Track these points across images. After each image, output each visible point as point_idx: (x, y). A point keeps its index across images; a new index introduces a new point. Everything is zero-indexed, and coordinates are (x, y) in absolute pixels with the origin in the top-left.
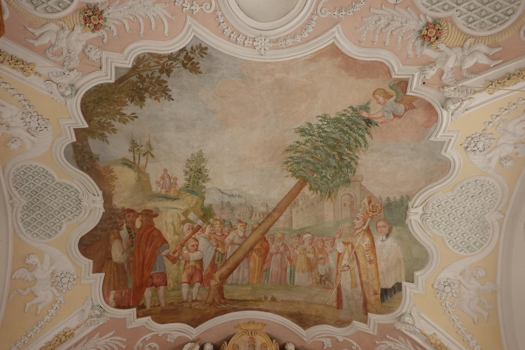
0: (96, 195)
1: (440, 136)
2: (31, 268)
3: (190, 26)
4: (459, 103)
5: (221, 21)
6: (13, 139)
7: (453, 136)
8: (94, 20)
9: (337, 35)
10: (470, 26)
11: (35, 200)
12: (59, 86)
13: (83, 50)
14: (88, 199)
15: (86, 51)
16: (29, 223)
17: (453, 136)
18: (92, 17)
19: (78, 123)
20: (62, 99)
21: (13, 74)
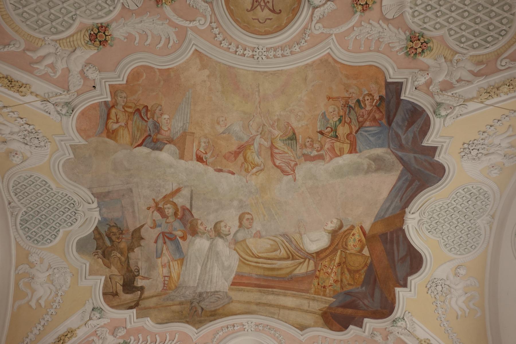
0: (91, 202)
1: (432, 141)
2: (32, 265)
3: (190, 41)
4: (450, 110)
5: (221, 39)
6: (11, 153)
7: (445, 142)
8: (101, 37)
9: (332, 46)
10: (462, 45)
11: (45, 191)
12: (56, 105)
13: (82, 70)
14: (83, 207)
15: (85, 71)
16: (38, 212)
17: (445, 142)
18: (99, 36)
19: (73, 140)
20: (59, 118)
21: (12, 96)
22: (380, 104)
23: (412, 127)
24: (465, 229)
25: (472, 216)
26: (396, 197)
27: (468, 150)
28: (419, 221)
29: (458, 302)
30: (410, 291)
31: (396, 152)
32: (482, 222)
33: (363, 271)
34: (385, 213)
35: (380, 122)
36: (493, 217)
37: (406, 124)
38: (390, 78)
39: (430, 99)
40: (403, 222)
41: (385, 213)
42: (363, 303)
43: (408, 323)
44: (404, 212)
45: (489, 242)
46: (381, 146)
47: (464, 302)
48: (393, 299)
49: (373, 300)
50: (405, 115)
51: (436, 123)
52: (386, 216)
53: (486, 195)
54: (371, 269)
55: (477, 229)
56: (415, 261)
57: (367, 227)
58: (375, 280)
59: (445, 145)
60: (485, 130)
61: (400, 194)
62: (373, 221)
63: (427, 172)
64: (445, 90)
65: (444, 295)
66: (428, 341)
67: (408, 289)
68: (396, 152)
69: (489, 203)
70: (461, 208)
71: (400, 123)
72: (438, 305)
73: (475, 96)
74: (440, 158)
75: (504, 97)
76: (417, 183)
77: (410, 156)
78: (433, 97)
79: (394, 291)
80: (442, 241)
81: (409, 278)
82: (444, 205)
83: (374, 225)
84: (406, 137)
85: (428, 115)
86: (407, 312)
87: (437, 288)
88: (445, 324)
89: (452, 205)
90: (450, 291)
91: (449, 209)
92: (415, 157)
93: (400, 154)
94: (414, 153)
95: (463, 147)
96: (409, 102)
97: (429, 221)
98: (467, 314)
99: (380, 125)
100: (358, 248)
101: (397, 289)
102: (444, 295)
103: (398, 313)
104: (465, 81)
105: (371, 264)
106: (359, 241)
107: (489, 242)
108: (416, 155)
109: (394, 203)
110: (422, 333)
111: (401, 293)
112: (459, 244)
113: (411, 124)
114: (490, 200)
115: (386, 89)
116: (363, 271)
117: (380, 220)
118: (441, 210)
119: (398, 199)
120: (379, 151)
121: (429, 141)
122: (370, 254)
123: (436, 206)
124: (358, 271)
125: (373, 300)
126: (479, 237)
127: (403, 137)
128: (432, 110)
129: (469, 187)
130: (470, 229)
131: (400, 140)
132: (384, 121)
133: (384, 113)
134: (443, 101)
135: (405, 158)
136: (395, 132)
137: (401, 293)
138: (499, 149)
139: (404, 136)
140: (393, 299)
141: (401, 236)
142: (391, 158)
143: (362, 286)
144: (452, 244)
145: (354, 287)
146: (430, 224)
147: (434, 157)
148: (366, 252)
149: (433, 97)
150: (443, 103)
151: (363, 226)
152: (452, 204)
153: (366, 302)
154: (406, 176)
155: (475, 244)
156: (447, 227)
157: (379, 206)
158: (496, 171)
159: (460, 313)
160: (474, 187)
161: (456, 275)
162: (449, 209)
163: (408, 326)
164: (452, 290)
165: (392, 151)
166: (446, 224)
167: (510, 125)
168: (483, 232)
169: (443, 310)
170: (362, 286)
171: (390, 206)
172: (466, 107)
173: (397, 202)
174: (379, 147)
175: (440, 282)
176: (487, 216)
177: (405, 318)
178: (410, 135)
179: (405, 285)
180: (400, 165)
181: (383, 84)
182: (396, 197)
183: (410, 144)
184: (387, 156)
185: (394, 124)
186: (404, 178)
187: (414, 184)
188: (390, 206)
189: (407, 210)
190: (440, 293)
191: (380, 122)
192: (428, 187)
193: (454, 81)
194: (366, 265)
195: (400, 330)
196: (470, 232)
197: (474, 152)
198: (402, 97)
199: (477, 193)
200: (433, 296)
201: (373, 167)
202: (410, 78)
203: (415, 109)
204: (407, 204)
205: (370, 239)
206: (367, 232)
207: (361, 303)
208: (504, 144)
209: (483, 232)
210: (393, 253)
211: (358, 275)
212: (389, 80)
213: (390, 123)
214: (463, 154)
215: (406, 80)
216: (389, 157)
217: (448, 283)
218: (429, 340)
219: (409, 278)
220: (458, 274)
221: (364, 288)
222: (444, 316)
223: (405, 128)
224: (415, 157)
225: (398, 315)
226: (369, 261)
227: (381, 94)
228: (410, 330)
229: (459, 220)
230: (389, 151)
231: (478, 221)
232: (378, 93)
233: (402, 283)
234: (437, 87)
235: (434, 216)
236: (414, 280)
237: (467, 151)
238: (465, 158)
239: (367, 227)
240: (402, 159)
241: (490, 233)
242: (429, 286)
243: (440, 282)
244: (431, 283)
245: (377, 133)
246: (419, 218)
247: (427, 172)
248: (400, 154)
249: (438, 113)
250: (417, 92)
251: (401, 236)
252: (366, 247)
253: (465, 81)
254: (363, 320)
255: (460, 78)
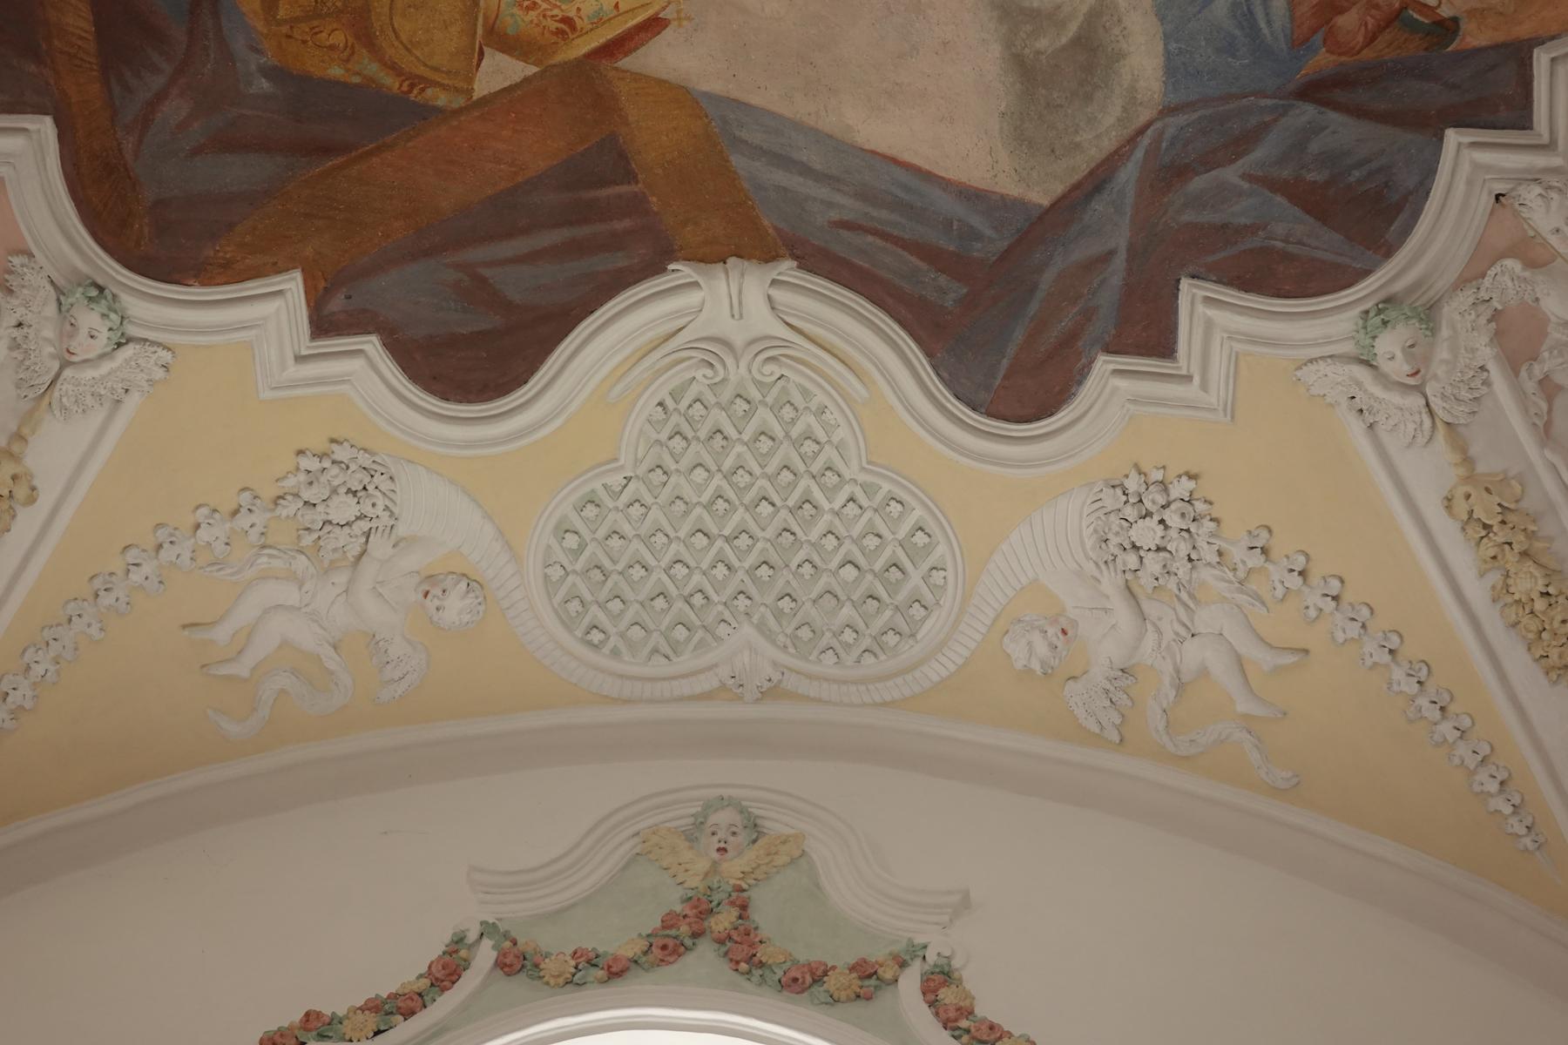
1: (1209, 325)
7: (1204, 386)
17: (1204, 386)
22: (1413, 26)
23: (1297, 211)
24: (697, 578)
25: (770, 600)
26: (864, 195)
27: (1162, 500)
28: (726, 344)
29: (284, 614)
30: (300, 359)
31: (1139, 154)
32: (746, 649)
33: (373, 69)
34: (759, 152)
35: (1319, 37)
36: (773, 692)
37: (1311, 176)
38: (1553, 60)
39: (1451, 275)
40: (711, 255)
41: (759, 152)
42: (161, 96)
43: (106, 367)
44: (767, 255)
45: (627, 701)
46: (1172, 70)
47: (285, 644)
48: (227, 265)
49: (196, 151)
50: (1359, 165)
51: (1329, 322)
52: (737, 161)
53: (891, 639)
54: (391, 114)
55: (700, 634)
56: (477, 357)
57: (663, 58)
58: (326, 150)
59: (1192, 391)
60: (1274, 554)
61: (884, 214)
62: (705, 87)
63: (1019, 335)
64: (1498, 337)
65: (308, 540)
66: (21, 492)
67: (307, 346)
68: (1139, 154)
69: (849, 659)
70: (814, 535)
71: (1314, 147)
72: (243, 521)
73: (1481, 468)
74: (1110, 385)
75: (1477, 591)
76: (950, 292)
77: (1112, 229)
78: (1460, 284)
79: (278, 270)
80: (616, 480)
81: (372, 344)
82: (829, 453)
83: (679, 95)
84: (1231, 191)
85: (1366, 273)
86: (166, 356)
87: (343, 498)
88: (147, 569)
89: (830, 492)
90: (333, 567)
91: (805, 482)
92: (1111, 253)
93: (1128, 175)
94: (1131, 248)
95: (1171, 475)
96: (1430, 171)
97: (727, 394)
98: (224, 670)
99: (1300, 43)
100: (517, 20)
101: (293, 284)
102: (308, 540)
103: (149, 304)
104: (1550, 411)
105: (427, 113)
106: (567, 20)
107: (627, 701)
108: (1122, 256)
109: (823, 192)
110: (54, 452)
111: (282, 302)
112: (607, 563)
113: (1316, 202)
114: (868, 659)
115: (1496, 47)
116: (373, 69)
117: (712, 125)
118: (797, 444)
119: (849, 206)
120: (1142, 63)
121: (1206, 313)
122: (485, 100)
123: (822, 410)
124: (366, 37)
125: (196, 151)
126: (655, 651)
127: (1230, 174)
128: (1399, 286)
129: (941, 549)
130: (698, 600)
131: (1208, 162)
132: (1321, 61)
133: (1367, 54)
134: (1445, 332)
135: (1099, 205)
136: (1264, 128)
137: (282, 302)
138: (1169, 635)
139: (1235, 180)
140: (227, 265)
141: (621, 261)
142: (1100, 129)
143: (275, 73)
144: (601, 533)
145: (260, 26)
146: (710, 398)
147: (1109, 350)
148: (499, 72)
149: (1460, 284)
150: (1434, 331)
151: (668, 34)
152: (837, 488)
153: (175, 109)
154: (988, 232)
155: (613, 641)
156: (700, 489)
157: (801, 109)
158: (1042, 649)
159: (222, 634)
160: (937, 577)
161: (430, 584)
162: (805, 482)
163: (89, 374)
164: (341, 578)
165: (1141, 131)
166: (718, 480)
167: (1306, 651)
168: (685, 662)
169: (219, 547)
170: (275, 73)
171: (806, 170)
172: (1421, 440)
173: (830, 205)
174: (1168, 55)
175: (379, 510)
176: (775, 664)
177: (129, 351)
178: (1240, 212)
179: (322, 326)
180: (1059, 189)
181: (1523, 31)
182: (864, 195)
183: (1188, 217)
184: (1115, 110)
185: (1307, 112)
186: (976, 221)
187: (943, 280)
188: (806, 170)
189: (786, 269)
190: (315, 517)
191: (1319, 37)
192: (929, 355)
193: (1548, 363)
194: (415, 81)
195: (49, 332)
196: (680, 604)
197: (1147, 533)
198: (1452, 137)
199: (901, 597)
200: (290, 483)
201: (1042, 43)
202: (1556, 161)
203: (1398, 208)
204: (820, 260)
205: (587, 83)
206: (626, 63)
207: (157, 82)
208: (1194, 654)
209: (685, 662)
210: (510, 235)
211: (338, 38)
212: (1541, 59)
213: (1315, 91)
214: (1133, 484)
215: (1545, 139)
216: (1109, 120)
217: (380, 547)
218: (31, 500)
219: (374, 338)
220: (437, 591)
221: (265, 84)
222: (186, 556)
223: (1286, 173)
224: (1111, 253)
225: (136, 307)
226: (442, 99)
227: (1466, 26)
228: (63, 387)
229: (744, 541)
230: (1144, 116)
231: (747, 630)
232: (1472, 13)
233: (337, 304)
234: (1512, 292)
235: (763, 414)
236: (365, 371)
237: (1154, 498)
238: (1112, 499)
239: (663, 58)
240: (1098, 189)
241: (681, 699)
242: (341, 453)
243: (379, 510)
244: (365, 459)
245: (1253, 31)
246: (738, 340)
247: (1019, 335)
248: (1128, 175)
249: (1391, 314)
250: (1486, 201)
251: (621, 261)
252: (532, 70)
253: (1550, 411)
254: (40, 110)
255: (1560, 388)
